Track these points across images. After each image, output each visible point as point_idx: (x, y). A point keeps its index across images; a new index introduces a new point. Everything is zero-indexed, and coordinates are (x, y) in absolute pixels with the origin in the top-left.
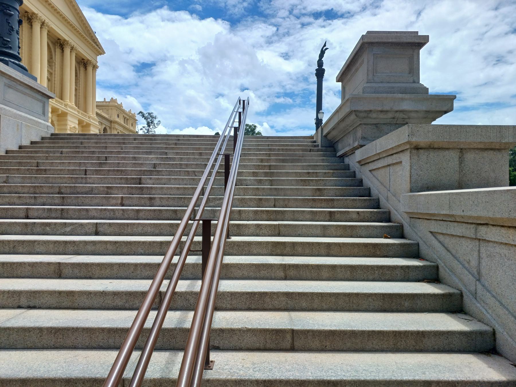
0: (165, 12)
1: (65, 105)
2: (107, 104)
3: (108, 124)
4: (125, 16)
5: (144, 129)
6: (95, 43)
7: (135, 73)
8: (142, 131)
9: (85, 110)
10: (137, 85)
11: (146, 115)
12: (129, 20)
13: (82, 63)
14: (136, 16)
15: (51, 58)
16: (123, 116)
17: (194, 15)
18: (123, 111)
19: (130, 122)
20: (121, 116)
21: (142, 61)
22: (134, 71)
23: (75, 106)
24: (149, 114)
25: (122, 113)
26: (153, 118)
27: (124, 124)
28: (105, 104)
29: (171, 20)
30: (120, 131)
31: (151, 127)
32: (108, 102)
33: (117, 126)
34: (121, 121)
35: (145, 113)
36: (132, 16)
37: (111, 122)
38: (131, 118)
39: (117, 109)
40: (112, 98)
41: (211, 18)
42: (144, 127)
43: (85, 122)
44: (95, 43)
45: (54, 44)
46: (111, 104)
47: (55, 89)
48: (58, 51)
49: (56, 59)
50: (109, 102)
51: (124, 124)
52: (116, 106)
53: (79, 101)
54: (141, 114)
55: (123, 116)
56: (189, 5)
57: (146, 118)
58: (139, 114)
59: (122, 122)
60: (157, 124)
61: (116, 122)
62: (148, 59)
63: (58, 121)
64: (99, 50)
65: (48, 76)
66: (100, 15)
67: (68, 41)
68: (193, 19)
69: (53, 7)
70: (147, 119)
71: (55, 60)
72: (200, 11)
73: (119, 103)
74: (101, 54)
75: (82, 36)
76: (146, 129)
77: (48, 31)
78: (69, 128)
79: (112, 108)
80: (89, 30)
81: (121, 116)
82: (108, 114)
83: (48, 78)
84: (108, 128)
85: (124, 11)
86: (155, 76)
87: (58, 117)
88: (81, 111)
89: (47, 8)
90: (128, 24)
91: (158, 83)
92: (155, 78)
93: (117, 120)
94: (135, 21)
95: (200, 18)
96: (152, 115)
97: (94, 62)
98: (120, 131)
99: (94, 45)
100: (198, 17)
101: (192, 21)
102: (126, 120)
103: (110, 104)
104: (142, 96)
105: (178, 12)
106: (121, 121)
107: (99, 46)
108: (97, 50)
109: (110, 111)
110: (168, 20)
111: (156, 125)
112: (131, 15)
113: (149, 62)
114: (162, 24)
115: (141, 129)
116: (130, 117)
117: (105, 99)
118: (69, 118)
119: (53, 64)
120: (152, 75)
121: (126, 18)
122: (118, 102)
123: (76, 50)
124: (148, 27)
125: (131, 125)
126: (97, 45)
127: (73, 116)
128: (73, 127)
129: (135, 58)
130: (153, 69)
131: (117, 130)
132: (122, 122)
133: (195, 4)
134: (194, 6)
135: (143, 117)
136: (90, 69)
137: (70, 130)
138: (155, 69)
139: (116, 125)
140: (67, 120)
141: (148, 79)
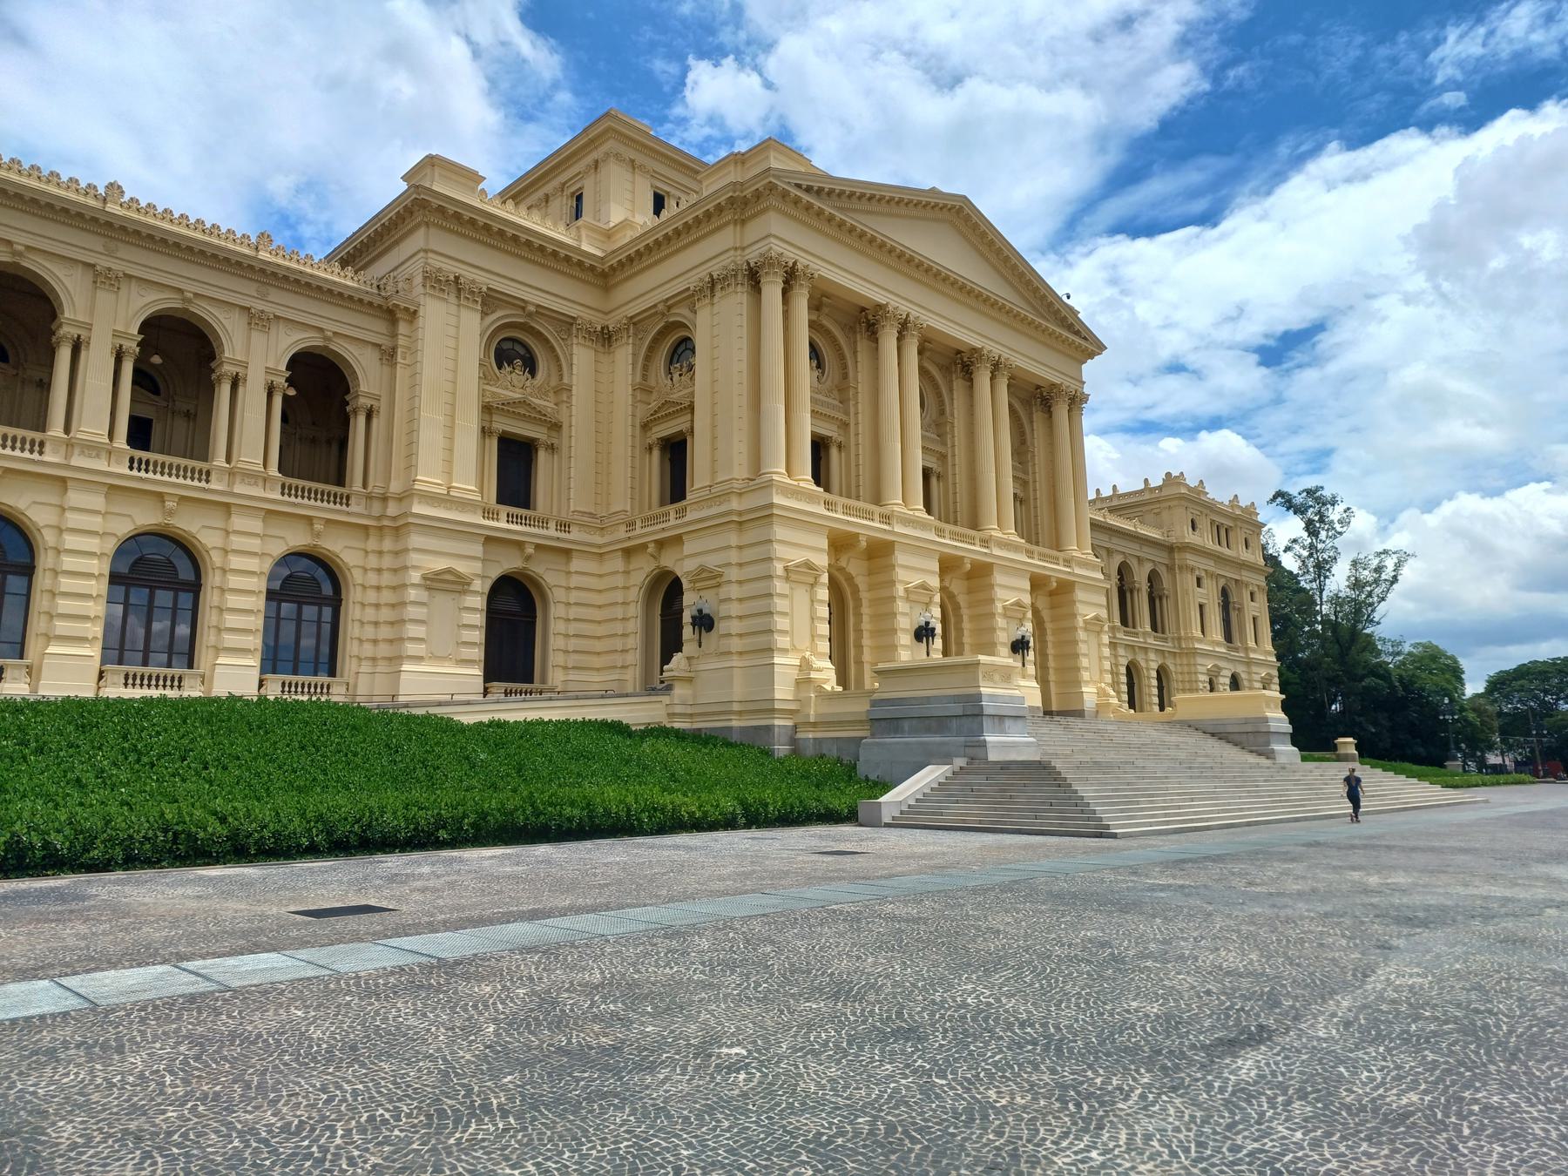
0: (1334, 160)
1: (982, 540)
2: (1153, 496)
3: (1161, 557)
4: (1209, 219)
5: (1297, 547)
6: (1069, 327)
7: (1264, 371)
8: (1290, 554)
9: (1057, 545)
10: (1278, 401)
11: (1299, 500)
12: (1226, 225)
13: (956, 364)
14: (1241, 207)
15: (1023, 442)
16: (1212, 522)
17: (1442, 130)
18: (1211, 507)
19: (1238, 537)
20: (1204, 524)
21: (1280, 329)
22: (1260, 364)
23: (926, 516)
24: (1310, 492)
25: (1205, 511)
26: (1324, 504)
27: (1217, 548)
28: (1147, 496)
29: (1362, 176)
30: (1203, 574)
31: (1323, 535)
32: (1156, 488)
33: (1191, 559)
34: (1205, 539)
35: (1296, 494)
36: (1232, 212)
37: (1170, 549)
38: (1239, 524)
39: (1186, 504)
40: (1168, 474)
41: (1513, 112)
42: (1295, 541)
43: (1053, 579)
44: (1069, 327)
45: (1027, 403)
46: (1165, 492)
47: (955, 497)
48: (1038, 416)
49: (956, 412)
50: (1160, 488)
51: (1217, 548)
52: (1182, 497)
53: (1036, 516)
54: (1279, 500)
55: (1212, 522)
56: (1416, 106)
57: (1299, 510)
58: (1275, 498)
59: (1209, 543)
60: (1340, 522)
61: (1186, 548)
62: (1296, 320)
63: (970, 591)
64: (1083, 343)
65: (1018, 492)
66: (1142, 244)
67: (982, 348)
68: (1437, 144)
69: (928, 270)
70: (1302, 513)
71: (952, 415)
72: (1461, 109)
73: (1193, 483)
74: (1091, 355)
75: (1031, 323)
76: (1304, 548)
77: (1010, 378)
78: (1000, 610)
79: (1172, 504)
80: (1045, 296)
81: (1204, 524)
82: (1159, 526)
83: (1015, 495)
84: (1163, 571)
85: (1199, 206)
86: (1328, 359)
87: (968, 579)
88: (948, 527)
89: (912, 278)
90: (1223, 237)
91: (1349, 378)
92: (1332, 368)
93: (1191, 538)
94: (1243, 224)
95: (1462, 129)
96: (1318, 494)
97: (1073, 386)
98: (1203, 574)
99: (1072, 337)
100: (1456, 129)
101: (1435, 150)
102: (1222, 532)
103: (1163, 494)
104: (1295, 432)
105: (1379, 144)
106: (1205, 539)
107: (1084, 334)
108: (1078, 347)
109: (1165, 515)
110: (1349, 180)
111: (1338, 527)
112: (1227, 212)
113: (1304, 325)
114: (1330, 199)
115: (1287, 549)
116: (1236, 519)
117: (1146, 481)
118: (999, 578)
119: (851, 392)
120: (1317, 361)
121: (1215, 225)
122: (1187, 482)
123: (1009, 367)
124: (1284, 226)
125: (1242, 546)
126: (1077, 333)
127: (919, 549)
128: (1012, 605)
129: (1253, 330)
130: (1319, 342)
131: (1193, 570)
132: (1209, 543)
133: (1439, 95)
134: (1432, 103)
135: (1288, 509)
136: (1061, 411)
137: (1021, 622)
138: (1325, 341)
139: (1188, 556)
140: (991, 586)
141: (1310, 375)
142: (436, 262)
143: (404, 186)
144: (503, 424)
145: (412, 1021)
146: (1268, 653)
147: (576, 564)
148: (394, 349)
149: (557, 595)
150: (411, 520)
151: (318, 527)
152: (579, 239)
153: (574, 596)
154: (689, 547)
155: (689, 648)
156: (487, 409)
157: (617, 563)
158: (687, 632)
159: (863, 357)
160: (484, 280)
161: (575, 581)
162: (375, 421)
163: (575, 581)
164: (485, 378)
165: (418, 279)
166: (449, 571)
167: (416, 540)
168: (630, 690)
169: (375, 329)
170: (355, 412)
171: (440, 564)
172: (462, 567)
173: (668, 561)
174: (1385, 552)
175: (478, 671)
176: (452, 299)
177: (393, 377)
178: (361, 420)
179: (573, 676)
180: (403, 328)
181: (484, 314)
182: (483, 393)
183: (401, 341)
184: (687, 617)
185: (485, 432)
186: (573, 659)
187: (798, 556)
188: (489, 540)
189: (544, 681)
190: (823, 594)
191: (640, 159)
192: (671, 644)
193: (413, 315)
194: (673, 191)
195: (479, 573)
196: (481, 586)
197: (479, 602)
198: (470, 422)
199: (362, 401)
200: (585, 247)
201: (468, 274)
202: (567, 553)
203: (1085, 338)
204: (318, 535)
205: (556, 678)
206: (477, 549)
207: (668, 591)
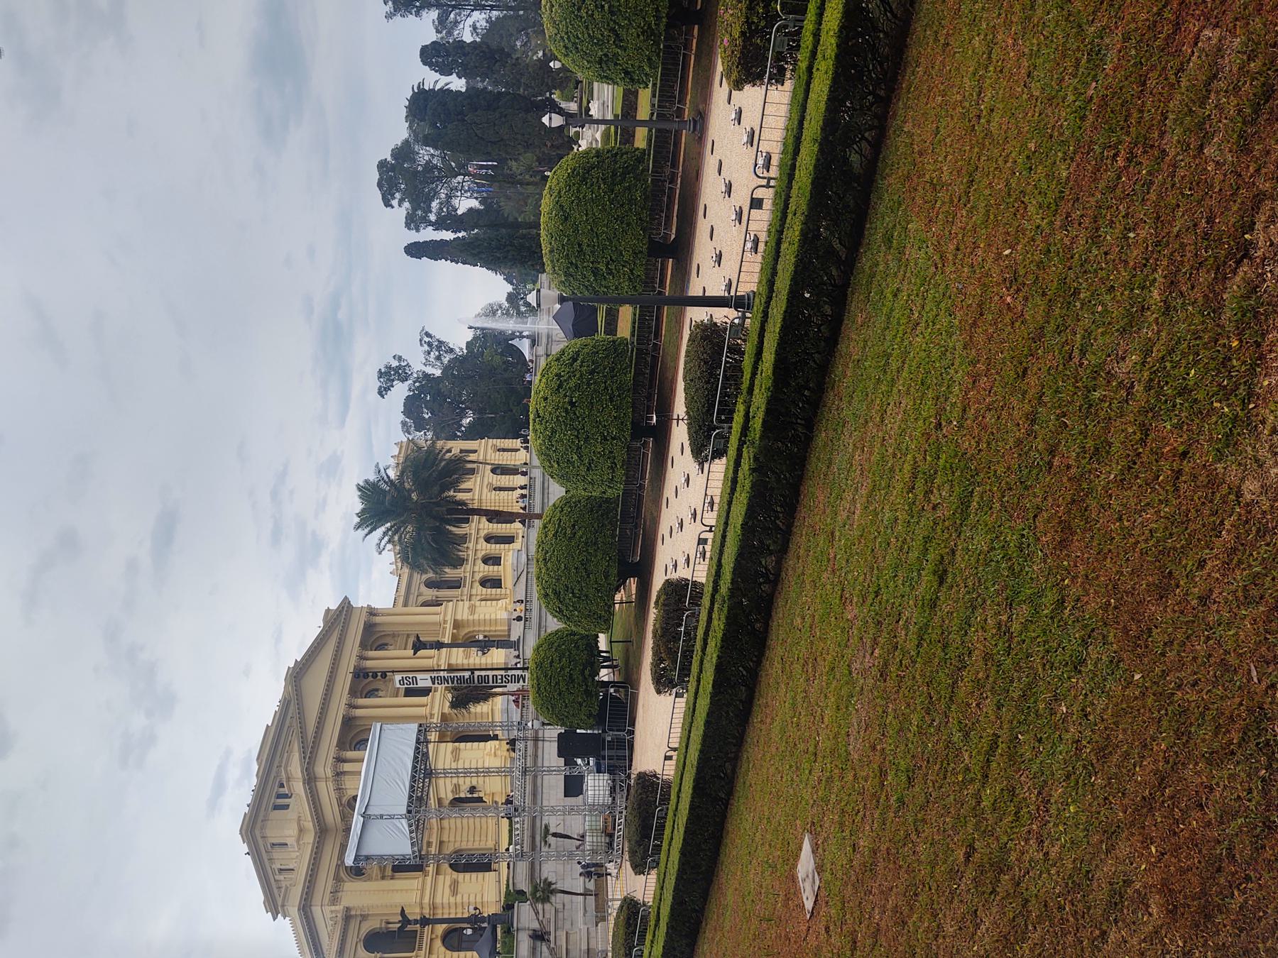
118: (459, 617)
136: (378, 619)
142: (326, 900)
143: (270, 913)
144: (389, 872)
145: (959, 405)
146: (480, 443)
147: (445, 838)
148: (361, 915)
149: (457, 846)
150: (426, 900)
151: (434, 936)
152: (308, 843)
153: (458, 838)
154: (442, 795)
155: (481, 795)
156: (383, 878)
157: (445, 823)
158: (475, 795)
159: (358, 723)
160: (331, 882)
161: (452, 839)
162: (391, 921)
163: (452, 839)
164: (370, 879)
165: (333, 908)
166: (450, 886)
167: (438, 900)
168: (442, 668)
169: (354, 925)
170: (387, 928)
171: (447, 890)
172: (448, 883)
173: (447, 802)
174: (421, 341)
175: (487, 874)
176: (340, 894)
177: (373, 915)
178: (390, 926)
179: (490, 838)
180: (353, 913)
181: (343, 881)
182: (376, 880)
183: (358, 913)
184: (470, 796)
185: (392, 878)
186: (483, 838)
187: (449, 756)
188: (438, 873)
189: (491, 849)
190: (462, 745)
191: (261, 818)
192: (480, 800)
193: (348, 909)
194: (272, 801)
195: (449, 875)
196: (455, 874)
197: (461, 875)
198: (388, 884)
199: (383, 926)
200: (311, 840)
201: (329, 889)
202: (441, 843)
203: (343, 608)
204: (437, 936)
205: (490, 844)
206: (441, 877)
207: (457, 802)
